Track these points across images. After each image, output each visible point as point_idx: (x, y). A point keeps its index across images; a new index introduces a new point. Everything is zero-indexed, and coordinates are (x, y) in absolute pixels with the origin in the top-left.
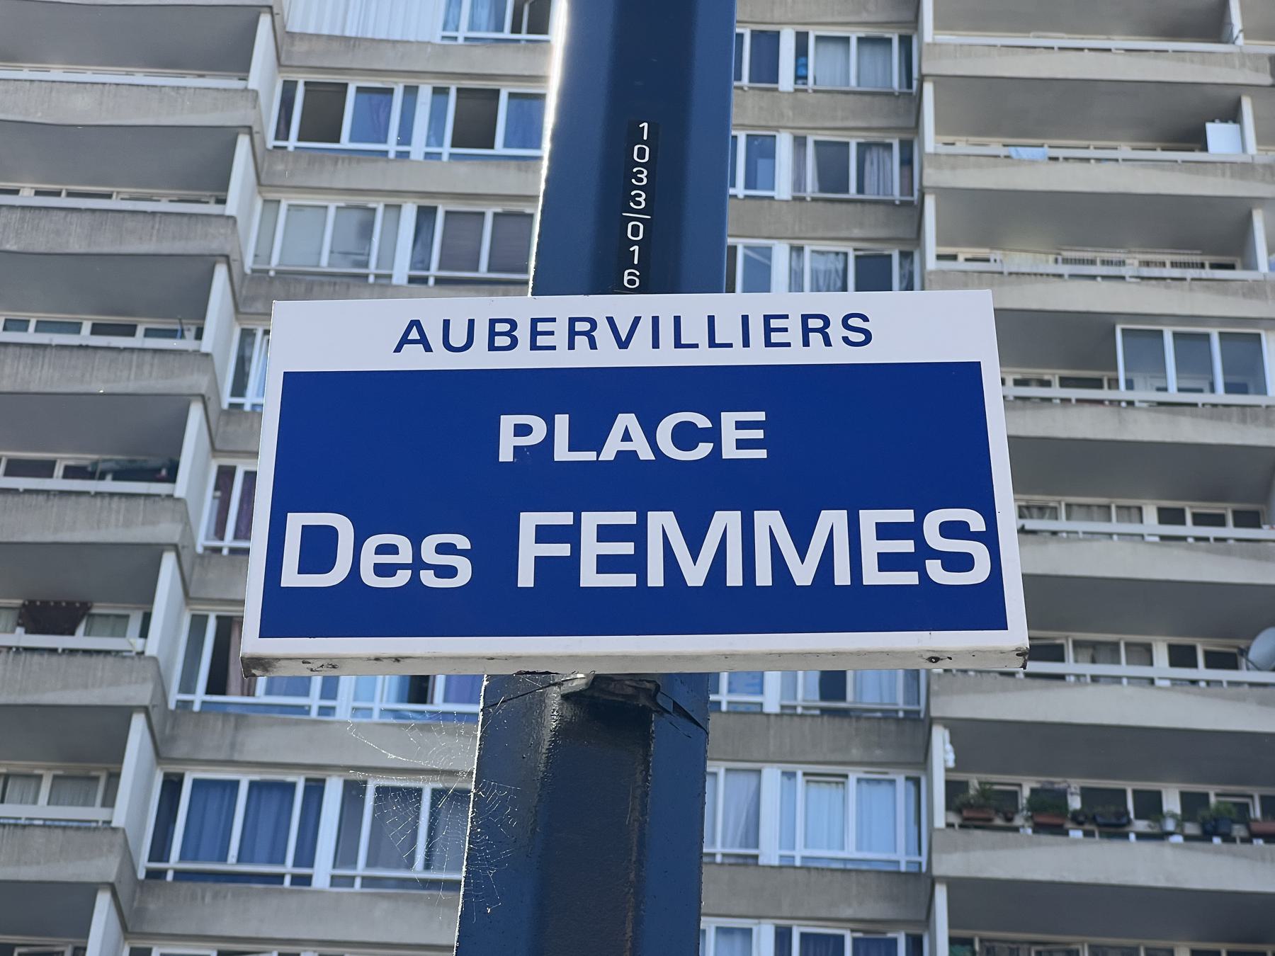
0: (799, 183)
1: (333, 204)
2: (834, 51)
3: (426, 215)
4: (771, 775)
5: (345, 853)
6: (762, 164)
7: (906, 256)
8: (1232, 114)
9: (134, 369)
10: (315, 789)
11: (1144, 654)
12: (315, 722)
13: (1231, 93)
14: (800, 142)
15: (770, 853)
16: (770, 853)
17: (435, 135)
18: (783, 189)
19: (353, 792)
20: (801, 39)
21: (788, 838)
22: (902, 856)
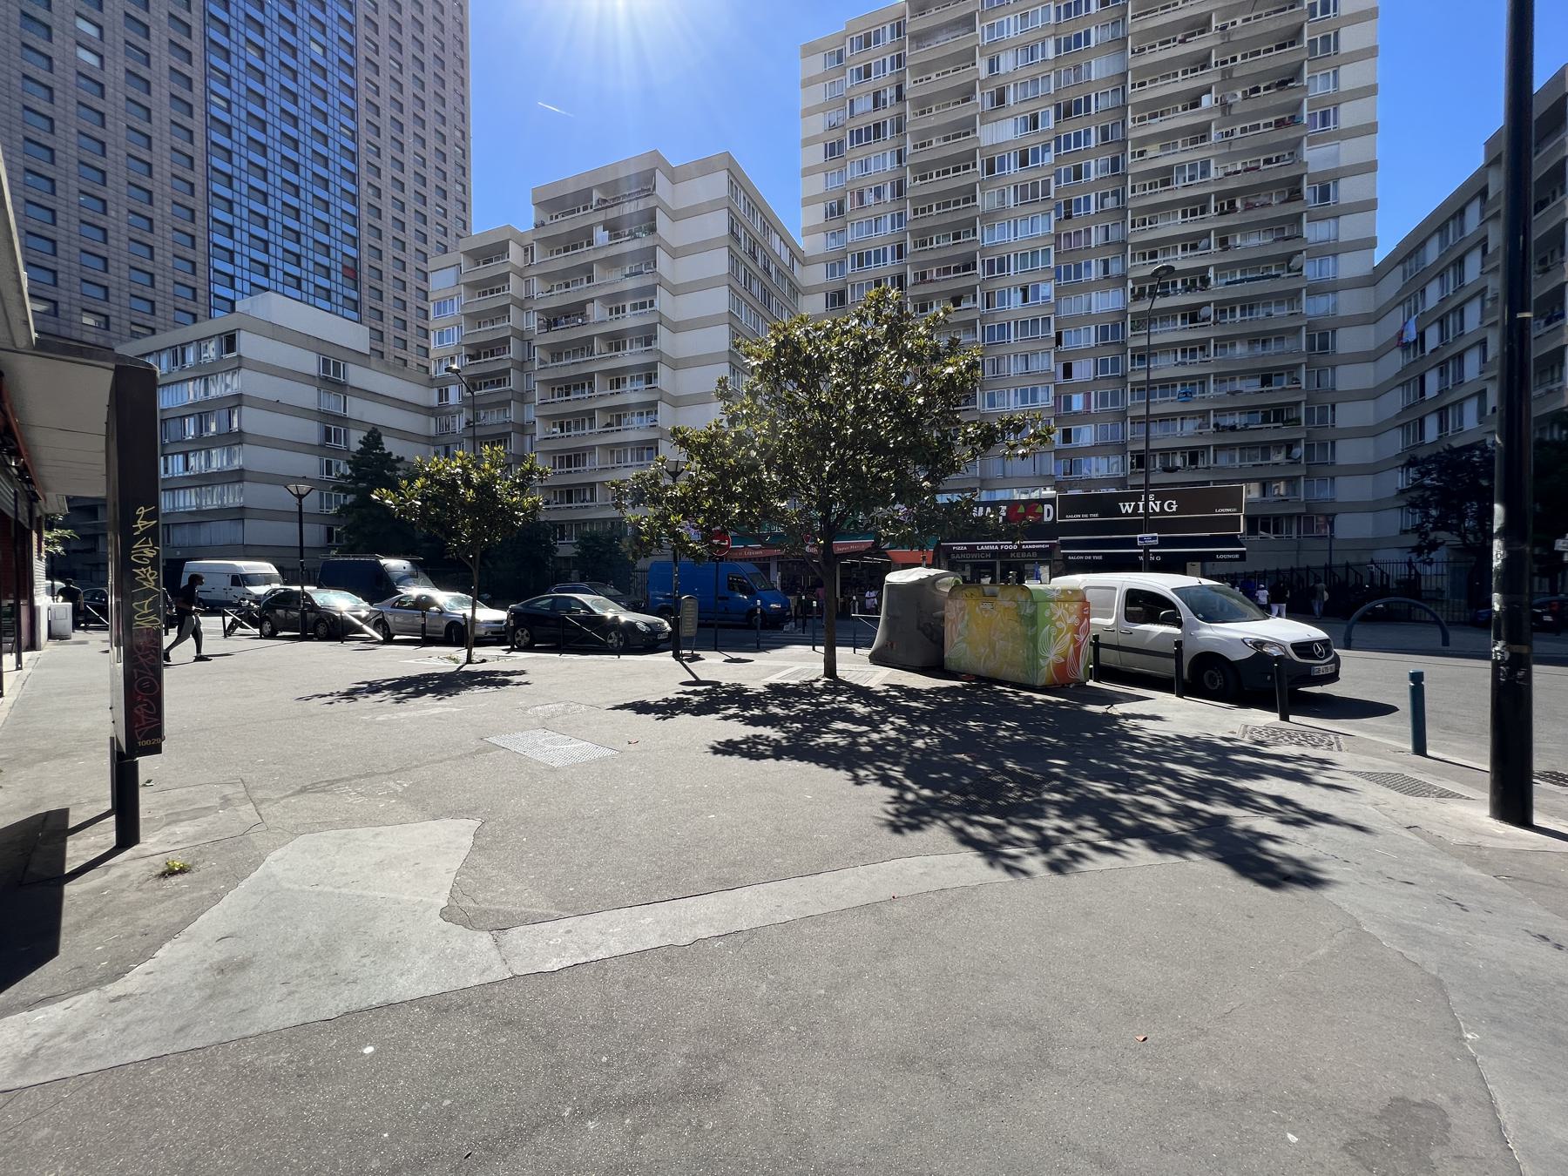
0: (1097, 141)
1: (996, 190)
2: (1105, 96)
3: (1016, 187)
4: (1094, 294)
5: (1016, 335)
6: (1087, 137)
7: (1123, 155)
8: (1209, 92)
9: (892, 818)
10: (1009, 324)
11: (1176, 75)
12: (1038, 5)
13: (1206, 52)
14: (1097, 128)
15: (1093, 312)
16: (1093, 312)
17: (1016, 166)
18: (1093, 145)
19: (1016, 323)
20: (1097, 95)
21: (1097, 307)
22: (1121, 306)
